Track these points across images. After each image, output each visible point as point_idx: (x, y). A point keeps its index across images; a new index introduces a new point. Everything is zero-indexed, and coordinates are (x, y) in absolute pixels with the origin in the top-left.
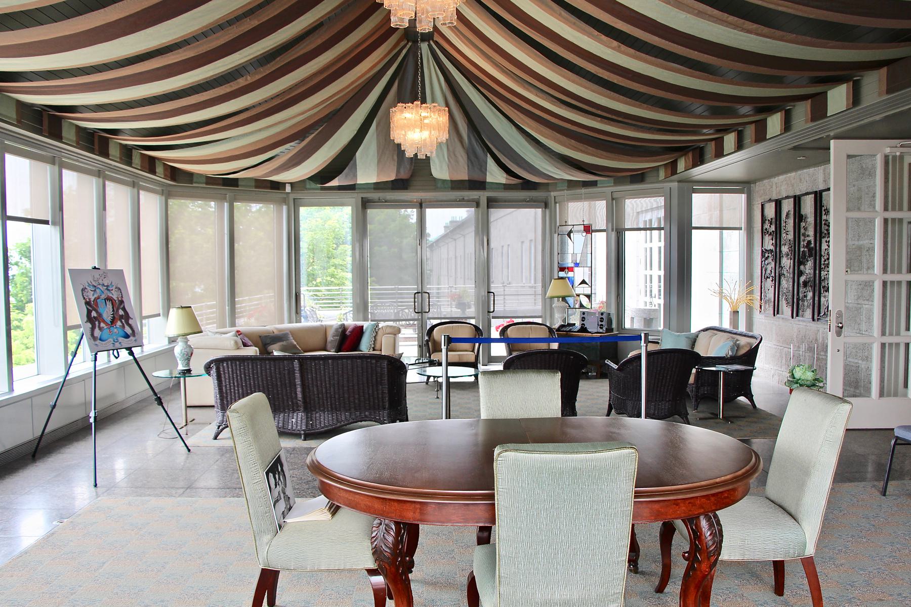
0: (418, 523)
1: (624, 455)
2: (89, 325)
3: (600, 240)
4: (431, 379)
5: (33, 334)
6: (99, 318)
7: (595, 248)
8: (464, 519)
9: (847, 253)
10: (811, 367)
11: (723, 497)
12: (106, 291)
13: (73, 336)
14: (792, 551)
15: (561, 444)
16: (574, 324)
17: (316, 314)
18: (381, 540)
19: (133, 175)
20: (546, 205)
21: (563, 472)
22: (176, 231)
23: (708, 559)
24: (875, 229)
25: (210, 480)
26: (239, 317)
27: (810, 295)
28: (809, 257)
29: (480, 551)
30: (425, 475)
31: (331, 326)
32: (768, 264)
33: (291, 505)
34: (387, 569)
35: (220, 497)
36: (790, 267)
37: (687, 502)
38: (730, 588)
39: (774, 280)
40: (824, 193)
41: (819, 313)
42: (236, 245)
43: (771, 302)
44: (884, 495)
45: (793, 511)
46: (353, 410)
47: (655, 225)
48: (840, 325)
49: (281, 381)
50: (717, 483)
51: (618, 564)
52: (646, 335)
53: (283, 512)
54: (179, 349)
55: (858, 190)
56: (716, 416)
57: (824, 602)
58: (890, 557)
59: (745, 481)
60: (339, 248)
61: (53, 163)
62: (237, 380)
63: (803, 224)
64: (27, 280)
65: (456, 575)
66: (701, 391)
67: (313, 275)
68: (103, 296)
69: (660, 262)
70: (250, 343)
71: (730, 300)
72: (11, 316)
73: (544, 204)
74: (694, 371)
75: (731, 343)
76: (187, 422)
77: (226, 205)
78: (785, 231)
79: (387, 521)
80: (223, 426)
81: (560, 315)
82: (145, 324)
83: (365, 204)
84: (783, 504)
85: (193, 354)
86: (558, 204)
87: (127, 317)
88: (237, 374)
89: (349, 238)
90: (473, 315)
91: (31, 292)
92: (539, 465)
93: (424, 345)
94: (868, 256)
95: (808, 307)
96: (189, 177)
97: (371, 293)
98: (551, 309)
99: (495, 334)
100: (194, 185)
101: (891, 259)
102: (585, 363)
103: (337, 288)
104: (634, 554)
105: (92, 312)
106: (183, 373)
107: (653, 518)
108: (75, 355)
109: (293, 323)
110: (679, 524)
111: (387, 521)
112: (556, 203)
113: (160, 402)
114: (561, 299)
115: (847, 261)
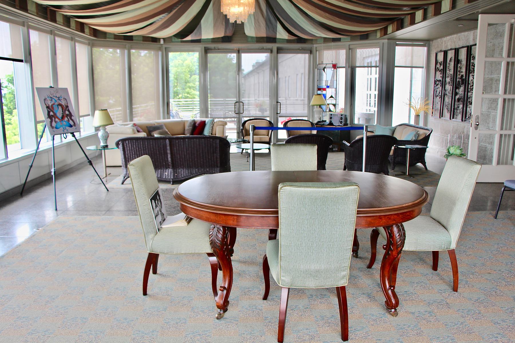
0: (236, 227)
1: (352, 190)
2: (49, 120)
3: (342, 73)
4: (244, 151)
5: (18, 128)
6: (54, 116)
7: (339, 78)
8: (261, 225)
9: (484, 82)
10: (459, 147)
11: (406, 215)
12: (58, 100)
13: (40, 127)
14: (443, 246)
15: (316, 183)
16: (326, 121)
17: (179, 115)
18: (215, 236)
19: (71, 34)
20: (311, 52)
21: (317, 198)
22: (98, 68)
23: (397, 249)
24: (501, 68)
25: (120, 206)
26: (136, 117)
27: (461, 106)
28: (462, 84)
29: (270, 244)
30: (240, 201)
31: (187, 121)
32: (438, 88)
33: (165, 218)
34: (218, 252)
35: (126, 216)
36: (450, 90)
37: (387, 217)
38: (408, 266)
39: (441, 97)
40: (473, 47)
41: (466, 117)
42: (132, 76)
43: (438, 110)
44: (496, 218)
45: (445, 224)
46: (200, 168)
47: (374, 65)
48: (477, 123)
49: (159, 151)
50: (403, 207)
51: (347, 250)
52: (367, 127)
53: (160, 222)
54: (100, 134)
55: (493, 45)
56: (404, 173)
57: (459, 275)
58: (496, 251)
59: (419, 206)
60: (192, 77)
61: (24, 25)
62: (134, 151)
63: (459, 65)
64: (12, 97)
65: (257, 258)
66: (397, 159)
67: (177, 93)
68: (57, 103)
69: (376, 85)
70: (141, 130)
71: (415, 108)
72: (4, 117)
73: (310, 51)
74: (393, 148)
75: (415, 133)
76: (106, 175)
77: (126, 51)
78: (448, 69)
79: (218, 226)
80: (127, 176)
81: (318, 116)
82: (81, 120)
83: (207, 51)
84: (440, 220)
85: (109, 137)
86: (318, 52)
87: (70, 115)
88: (134, 147)
89: (198, 71)
90: (268, 115)
91: (15, 103)
92: (303, 194)
93: (240, 132)
94: (496, 84)
95: (460, 113)
96: (104, 35)
97: (210, 103)
98: (313, 112)
99: (280, 125)
100: (107, 39)
101: (509, 86)
102: (331, 142)
103: (191, 100)
104: (356, 247)
105: (50, 112)
106: (103, 147)
107: (367, 226)
108: (42, 137)
109: (165, 119)
110: (382, 230)
111: (218, 226)
112: (316, 51)
113: (91, 163)
114: (318, 106)
115: (484, 87)
